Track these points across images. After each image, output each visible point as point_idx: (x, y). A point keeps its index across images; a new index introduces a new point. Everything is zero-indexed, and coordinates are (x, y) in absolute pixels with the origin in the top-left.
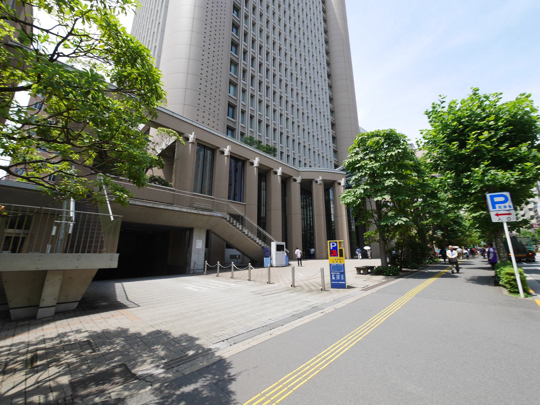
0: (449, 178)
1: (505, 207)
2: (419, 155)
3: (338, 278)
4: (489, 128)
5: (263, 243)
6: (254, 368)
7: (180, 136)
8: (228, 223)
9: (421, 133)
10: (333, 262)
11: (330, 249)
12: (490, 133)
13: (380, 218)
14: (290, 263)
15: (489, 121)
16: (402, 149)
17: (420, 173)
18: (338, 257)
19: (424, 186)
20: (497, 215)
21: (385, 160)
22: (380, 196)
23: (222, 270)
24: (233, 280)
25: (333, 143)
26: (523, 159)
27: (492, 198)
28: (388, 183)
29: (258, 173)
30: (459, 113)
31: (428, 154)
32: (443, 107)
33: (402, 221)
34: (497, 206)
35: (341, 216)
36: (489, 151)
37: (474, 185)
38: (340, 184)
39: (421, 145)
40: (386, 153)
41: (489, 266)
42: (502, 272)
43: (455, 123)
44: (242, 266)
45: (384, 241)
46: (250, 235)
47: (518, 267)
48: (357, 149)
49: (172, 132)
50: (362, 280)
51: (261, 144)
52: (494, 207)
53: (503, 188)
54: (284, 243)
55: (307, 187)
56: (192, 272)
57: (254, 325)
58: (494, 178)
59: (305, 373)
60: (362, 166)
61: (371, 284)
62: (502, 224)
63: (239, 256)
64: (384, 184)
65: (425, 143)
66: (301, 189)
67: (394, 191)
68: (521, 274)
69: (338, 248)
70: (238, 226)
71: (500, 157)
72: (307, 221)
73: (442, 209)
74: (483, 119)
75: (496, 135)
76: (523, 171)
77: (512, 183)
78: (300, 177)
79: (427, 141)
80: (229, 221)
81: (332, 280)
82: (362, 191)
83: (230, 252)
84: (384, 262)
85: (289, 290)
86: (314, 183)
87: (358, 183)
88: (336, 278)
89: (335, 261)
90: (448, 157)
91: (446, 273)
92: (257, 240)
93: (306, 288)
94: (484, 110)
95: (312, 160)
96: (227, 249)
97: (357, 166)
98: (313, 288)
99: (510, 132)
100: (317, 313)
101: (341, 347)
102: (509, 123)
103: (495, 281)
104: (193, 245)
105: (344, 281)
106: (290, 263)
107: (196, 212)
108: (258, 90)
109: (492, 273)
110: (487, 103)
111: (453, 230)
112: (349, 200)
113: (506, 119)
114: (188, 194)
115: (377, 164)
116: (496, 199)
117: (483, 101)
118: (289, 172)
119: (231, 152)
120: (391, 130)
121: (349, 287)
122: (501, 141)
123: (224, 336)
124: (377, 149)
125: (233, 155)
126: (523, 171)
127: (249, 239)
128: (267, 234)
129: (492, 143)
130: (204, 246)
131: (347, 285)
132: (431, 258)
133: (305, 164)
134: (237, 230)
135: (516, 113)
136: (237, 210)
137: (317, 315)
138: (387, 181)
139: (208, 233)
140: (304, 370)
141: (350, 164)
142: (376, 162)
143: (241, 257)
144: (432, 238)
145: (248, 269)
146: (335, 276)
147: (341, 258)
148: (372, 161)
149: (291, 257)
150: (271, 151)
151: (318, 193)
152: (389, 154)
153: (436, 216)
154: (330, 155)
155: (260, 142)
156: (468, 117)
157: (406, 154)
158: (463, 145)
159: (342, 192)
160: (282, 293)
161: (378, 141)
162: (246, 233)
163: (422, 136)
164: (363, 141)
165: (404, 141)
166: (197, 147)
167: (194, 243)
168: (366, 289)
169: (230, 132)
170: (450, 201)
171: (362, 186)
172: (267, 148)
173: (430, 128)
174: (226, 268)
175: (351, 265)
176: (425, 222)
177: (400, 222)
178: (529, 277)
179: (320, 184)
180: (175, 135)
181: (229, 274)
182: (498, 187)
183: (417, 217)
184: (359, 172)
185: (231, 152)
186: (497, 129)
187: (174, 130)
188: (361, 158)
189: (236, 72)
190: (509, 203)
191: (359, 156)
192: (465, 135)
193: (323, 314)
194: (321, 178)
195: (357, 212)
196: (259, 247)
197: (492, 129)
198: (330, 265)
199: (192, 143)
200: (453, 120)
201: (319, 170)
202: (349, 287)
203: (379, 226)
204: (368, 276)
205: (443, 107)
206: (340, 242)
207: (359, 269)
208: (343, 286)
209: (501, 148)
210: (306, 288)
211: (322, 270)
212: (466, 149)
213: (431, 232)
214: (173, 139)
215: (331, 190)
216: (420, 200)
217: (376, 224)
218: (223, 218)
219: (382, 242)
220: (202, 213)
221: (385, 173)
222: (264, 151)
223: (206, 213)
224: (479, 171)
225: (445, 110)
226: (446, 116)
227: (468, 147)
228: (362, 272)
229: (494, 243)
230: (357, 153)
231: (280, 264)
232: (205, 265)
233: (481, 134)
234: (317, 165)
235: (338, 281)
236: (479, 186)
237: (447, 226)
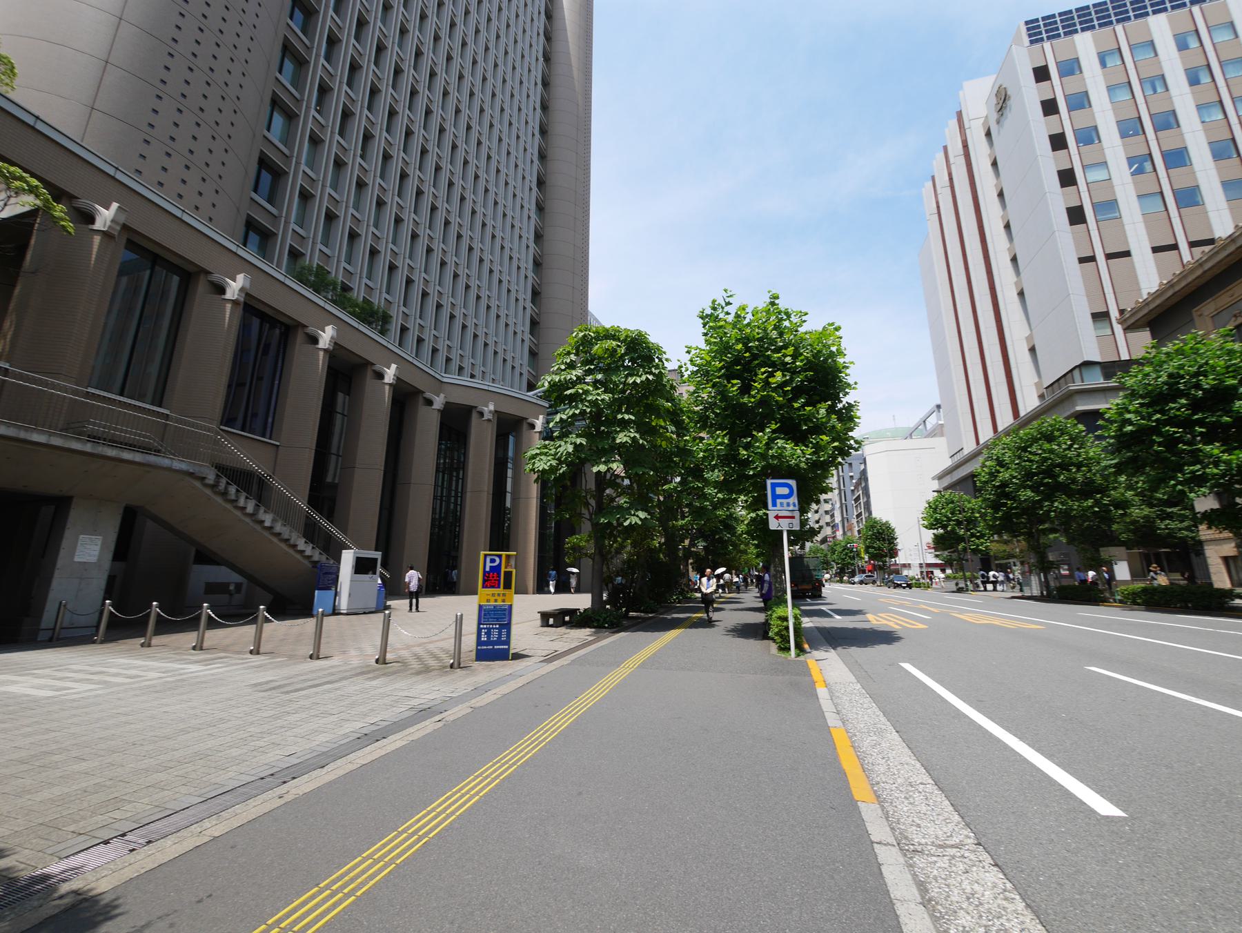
0: (720, 444)
1: (788, 505)
2: (684, 391)
3: (494, 637)
4: (784, 367)
5: (317, 551)
6: (199, 902)
7: (57, 199)
8: (208, 492)
9: (688, 352)
10: (488, 601)
11: (484, 571)
12: (784, 376)
13: (601, 509)
14: (389, 603)
15: (785, 356)
16: (654, 374)
17: (679, 425)
18: (501, 590)
19: (684, 452)
20: (777, 517)
21: (623, 391)
22: (605, 463)
23: (164, 627)
24: (201, 656)
25: (532, 333)
26: (818, 429)
27: (774, 486)
28: (622, 438)
29: (329, 367)
30: (748, 330)
31: (695, 392)
32: (728, 313)
33: (638, 517)
34: (779, 501)
35: (528, 498)
36: (780, 407)
37: (753, 462)
38: (532, 426)
39: (686, 374)
40: (627, 377)
41: (762, 605)
42: (775, 615)
43: (740, 346)
44: (236, 612)
45: (603, 555)
46: (278, 528)
47: (794, 606)
48: (573, 357)
49: (21, 179)
50: (548, 639)
51: (349, 295)
52: (774, 505)
53: (791, 472)
54: (378, 555)
55: (456, 423)
56: (42, 636)
57: (230, 778)
58: (780, 455)
59: (352, 880)
60: (577, 394)
61: (561, 646)
62: (781, 532)
63: (238, 586)
64: (614, 439)
65: (693, 373)
66: (442, 424)
67: (630, 455)
68: (796, 618)
69: (503, 570)
70: (242, 502)
71: (792, 418)
72: (448, 502)
73: (706, 499)
74: (778, 350)
75: (792, 380)
76: (818, 448)
77: (803, 465)
78: (442, 395)
79: (695, 369)
80: (213, 487)
81: (479, 642)
82: (570, 449)
83: (203, 574)
84: (597, 600)
85: (369, 672)
86: (474, 415)
87: (566, 429)
88: (489, 637)
89: (492, 599)
90: (723, 405)
91: (700, 618)
92: (301, 544)
93: (416, 665)
94: (781, 334)
95: (479, 360)
96: (197, 568)
97: (568, 392)
98: (432, 663)
99: (810, 380)
100: (427, 722)
101: (463, 796)
102: (810, 365)
103: (759, 632)
104: (62, 553)
105: (508, 642)
106: (389, 603)
107: (88, 448)
108: (359, 152)
109: (759, 618)
110: (786, 323)
111: (721, 540)
112: (542, 464)
113: (807, 358)
114: (63, 389)
115: (607, 397)
116: (780, 491)
117: (781, 320)
118: (416, 381)
119: (247, 294)
120: (640, 332)
121: (517, 656)
122: (797, 392)
123: (116, 826)
124: (611, 365)
125: (253, 303)
126: (818, 448)
127: (275, 540)
128: (334, 530)
129: (785, 393)
130: (109, 556)
131: (512, 652)
132: (682, 593)
133: (461, 368)
134: (238, 513)
135: (819, 352)
136: (244, 453)
137: (428, 726)
138: (621, 435)
139: (130, 520)
140: (352, 875)
141: (553, 385)
142: (605, 392)
143: (244, 587)
144: (688, 553)
145: (254, 621)
146: (488, 634)
147: (507, 591)
148: (597, 388)
149: (394, 588)
150: (374, 317)
151: (482, 440)
152: (630, 380)
153: (698, 513)
154: (522, 359)
155: (346, 288)
156: (758, 340)
157: (659, 388)
158: (746, 389)
159: (535, 444)
160: (345, 682)
161: (614, 351)
162: (267, 524)
163: (689, 357)
164: (586, 343)
165: (660, 360)
166: (123, 254)
167: (65, 543)
168: (550, 659)
169: (254, 238)
170: (720, 486)
171: (573, 438)
172: (362, 309)
173: (703, 345)
174: (179, 617)
175: (527, 609)
176: (680, 522)
177: (634, 520)
178: (807, 622)
179: (489, 420)
180: (32, 190)
181: (190, 638)
182: (782, 470)
183: (669, 510)
184: (571, 407)
185: (247, 294)
186: (794, 372)
187: (33, 175)
188: (578, 378)
189: (298, 81)
190: (794, 499)
191: (574, 373)
192: (750, 372)
193: (440, 724)
194: (492, 407)
195: (561, 489)
196: (306, 562)
197: (788, 370)
198: (480, 607)
199: (106, 235)
200: (738, 341)
201: (491, 387)
202: (517, 656)
203: (596, 525)
204: (562, 630)
205: (728, 313)
206: (508, 557)
207: (545, 616)
208: (503, 656)
209: (796, 405)
210: (416, 665)
211: (459, 621)
212: (750, 396)
213: (687, 542)
214: (25, 203)
215: (511, 438)
216: (678, 479)
217: (590, 520)
218: (191, 474)
219: (597, 558)
220: (111, 452)
221: (620, 416)
222: (353, 314)
223: (127, 455)
224: (763, 436)
225: (730, 318)
226: (728, 329)
227: (753, 393)
228: (551, 621)
229: (772, 569)
230: (571, 366)
231: (360, 606)
232: (101, 613)
233: (771, 375)
234: (490, 376)
235: (494, 643)
236: (759, 464)
237: (714, 532)
